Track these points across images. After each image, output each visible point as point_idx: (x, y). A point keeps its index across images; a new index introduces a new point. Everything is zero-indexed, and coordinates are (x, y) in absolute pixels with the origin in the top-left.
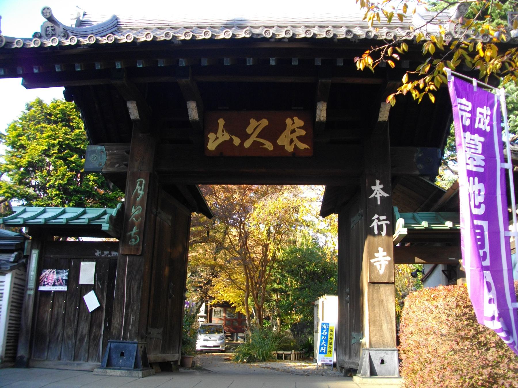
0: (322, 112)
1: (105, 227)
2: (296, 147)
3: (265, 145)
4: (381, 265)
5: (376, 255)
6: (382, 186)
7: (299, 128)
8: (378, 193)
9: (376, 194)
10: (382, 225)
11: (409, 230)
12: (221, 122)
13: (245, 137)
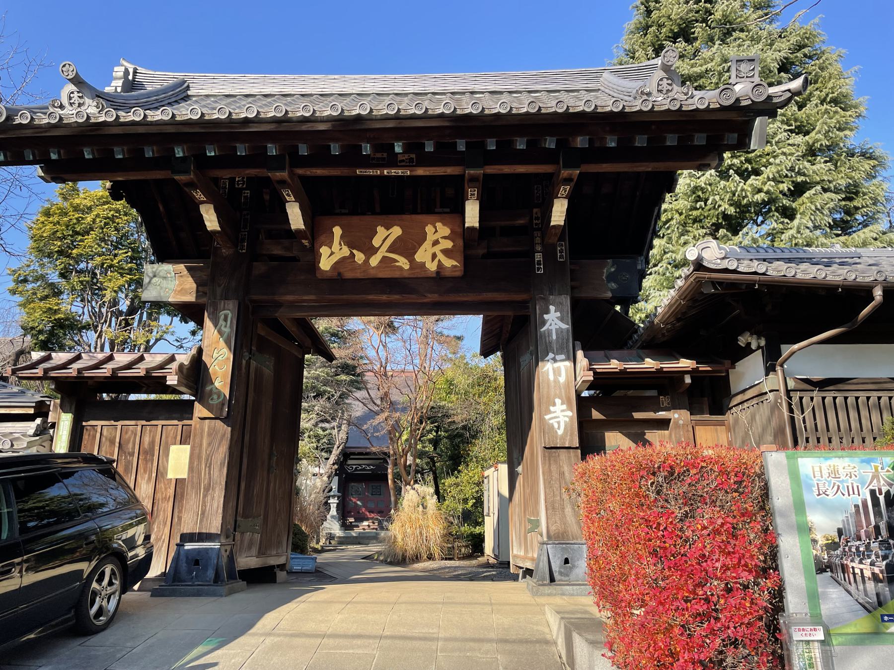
0: (472, 214)
1: (172, 380)
4: (559, 423)
5: (552, 408)
6: (558, 314)
7: (445, 238)
10: (559, 368)
11: (595, 373)
12: (337, 231)
13: (371, 251)
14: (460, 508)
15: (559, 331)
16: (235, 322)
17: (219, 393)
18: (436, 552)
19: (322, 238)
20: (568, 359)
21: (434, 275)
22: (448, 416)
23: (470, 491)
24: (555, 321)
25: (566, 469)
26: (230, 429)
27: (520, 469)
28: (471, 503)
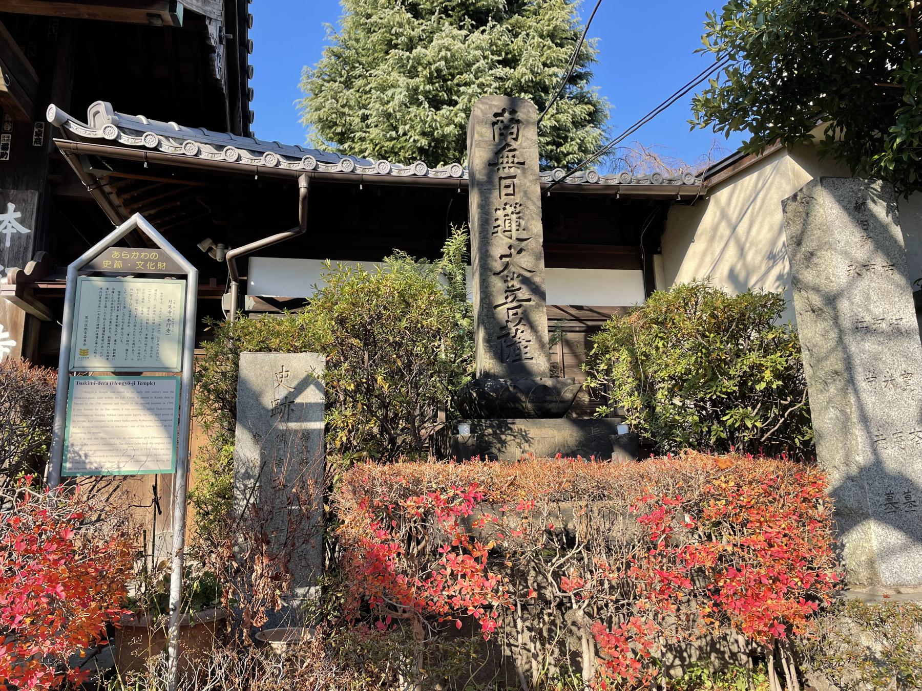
8: (9, 226)
15: (16, 237)
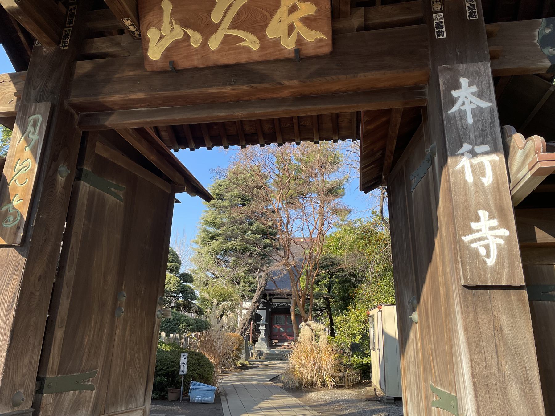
2: (300, 41)
3: (243, 40)
4: (487, 247)
5: (474, 225)
6: (474, 89)
8: (467, 102)
9: (463, 104)
13: (208, 29)
14: (349, 341)
15: (478, 112)
16: (44, 128)
17: (16, 213)
18: (329, 381)
19: (150, 17)
20: (494, 150)
21: (293, 55)
22: (337, 265)
23: (357, 328)
24: (469, 98)
25: (504, 321)
26: (24, 259)
27: (415, 316)
28: (359, 337)
